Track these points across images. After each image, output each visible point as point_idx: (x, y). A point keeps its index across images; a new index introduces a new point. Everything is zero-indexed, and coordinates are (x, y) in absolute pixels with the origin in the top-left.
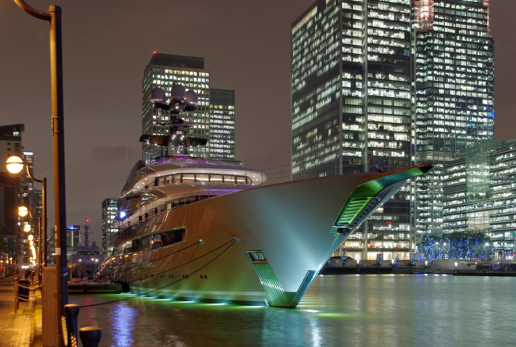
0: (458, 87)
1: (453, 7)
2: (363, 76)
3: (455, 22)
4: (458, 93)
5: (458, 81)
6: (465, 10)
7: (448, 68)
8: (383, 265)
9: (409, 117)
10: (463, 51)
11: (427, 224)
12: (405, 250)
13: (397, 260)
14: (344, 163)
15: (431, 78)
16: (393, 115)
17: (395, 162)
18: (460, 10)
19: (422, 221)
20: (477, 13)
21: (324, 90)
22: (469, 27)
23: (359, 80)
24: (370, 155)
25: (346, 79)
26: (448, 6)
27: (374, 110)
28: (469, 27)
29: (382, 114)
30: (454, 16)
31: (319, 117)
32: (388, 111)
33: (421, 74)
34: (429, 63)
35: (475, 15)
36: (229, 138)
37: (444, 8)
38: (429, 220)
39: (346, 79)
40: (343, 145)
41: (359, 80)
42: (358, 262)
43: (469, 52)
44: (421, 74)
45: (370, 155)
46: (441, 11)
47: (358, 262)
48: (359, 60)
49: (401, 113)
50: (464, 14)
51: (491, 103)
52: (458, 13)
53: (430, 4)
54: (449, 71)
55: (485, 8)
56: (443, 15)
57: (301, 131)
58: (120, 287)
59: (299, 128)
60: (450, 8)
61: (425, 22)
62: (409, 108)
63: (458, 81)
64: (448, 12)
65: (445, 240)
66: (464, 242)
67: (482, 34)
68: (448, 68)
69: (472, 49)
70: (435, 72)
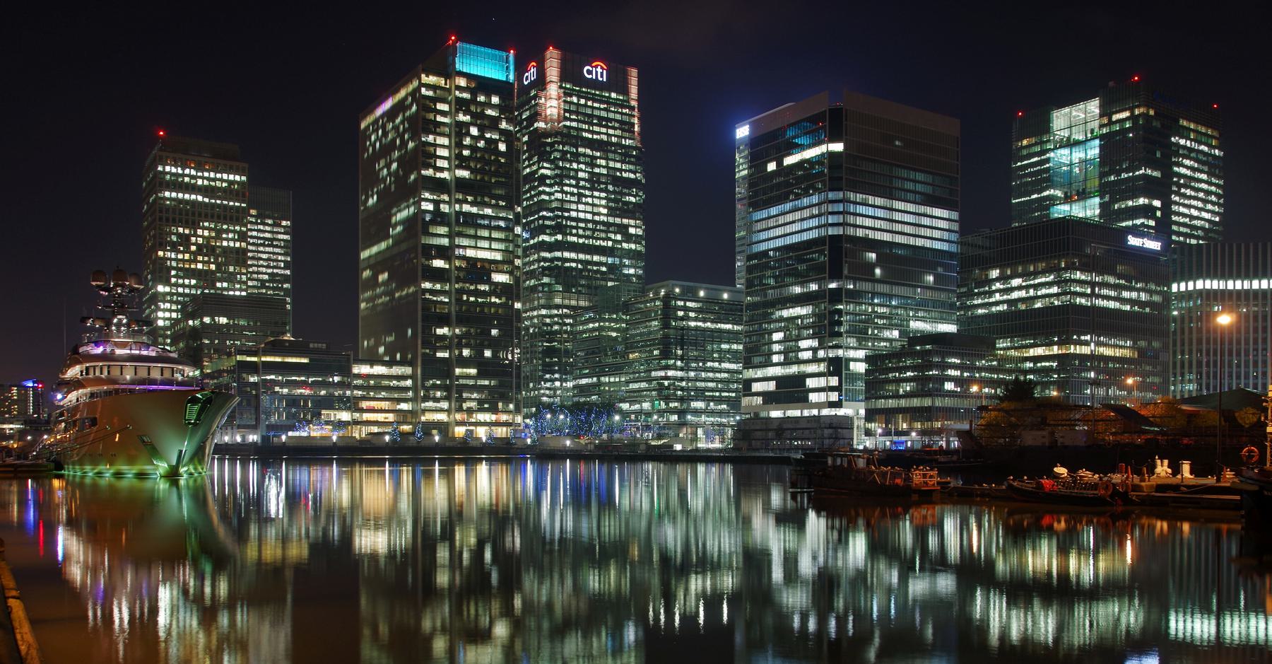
0: (596, 210)
1: (590, 103)
2: (450, 196)
3: (593, 124)
4: (597, 218)
5: (596, 201)
6: (605, 109)
7: (582, 183)
8: (474, 443)
9: (512, 252)
10: (603, 162)
11: (555, 389)
12: (506, 424)
13: (490, 437)
14: (423, 309)
15: (559, 196)
16: (490, 249)
17: (493, 310)
18: (599, 109)
19: (548, 385)
20: (622, 114)
21: (400, 211)
22: (611, 132)
23: (444, 202)
24: (459, 300)
25: (427, 200)
26: (583, 101)
27: (465, 242)
28: (611, 132)
29: (476, 247)
30: (592, 116)
31: (393, 245)
32: (486, 244)
33: (547, 189)
34: (557, 175)
35: (618, 117)
36: (468, 139)
37: (578, 105)
38: (558, 384)
39: (427, 200)
40: (197, 373)
41: (444, 202)
42: (484, 440)
43: (611, 164)
44: (547, 189)
45: (459, 300)
46: (573, 108)
47: (484, 440)
48: (445, 175)
49: (502, 246)
50: (603, 114)
51: (640, 232)
52: (596, 113)
53: (559, 98)
54: (584, 188)
55: (632, 108)
56: (577, 113)
57: (372, 262)
58: (52, 465)
59: (370, 257)
60: (586, 106)
61: (552, 120)
62: (512, 241)
63: (596, 201)
64: (582, 110)
65: (562, 412)
66: (589, 415)
67: (628, 142)
68: (582, 183)
69: (615, 160)
70: (566, 188)
